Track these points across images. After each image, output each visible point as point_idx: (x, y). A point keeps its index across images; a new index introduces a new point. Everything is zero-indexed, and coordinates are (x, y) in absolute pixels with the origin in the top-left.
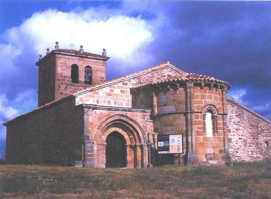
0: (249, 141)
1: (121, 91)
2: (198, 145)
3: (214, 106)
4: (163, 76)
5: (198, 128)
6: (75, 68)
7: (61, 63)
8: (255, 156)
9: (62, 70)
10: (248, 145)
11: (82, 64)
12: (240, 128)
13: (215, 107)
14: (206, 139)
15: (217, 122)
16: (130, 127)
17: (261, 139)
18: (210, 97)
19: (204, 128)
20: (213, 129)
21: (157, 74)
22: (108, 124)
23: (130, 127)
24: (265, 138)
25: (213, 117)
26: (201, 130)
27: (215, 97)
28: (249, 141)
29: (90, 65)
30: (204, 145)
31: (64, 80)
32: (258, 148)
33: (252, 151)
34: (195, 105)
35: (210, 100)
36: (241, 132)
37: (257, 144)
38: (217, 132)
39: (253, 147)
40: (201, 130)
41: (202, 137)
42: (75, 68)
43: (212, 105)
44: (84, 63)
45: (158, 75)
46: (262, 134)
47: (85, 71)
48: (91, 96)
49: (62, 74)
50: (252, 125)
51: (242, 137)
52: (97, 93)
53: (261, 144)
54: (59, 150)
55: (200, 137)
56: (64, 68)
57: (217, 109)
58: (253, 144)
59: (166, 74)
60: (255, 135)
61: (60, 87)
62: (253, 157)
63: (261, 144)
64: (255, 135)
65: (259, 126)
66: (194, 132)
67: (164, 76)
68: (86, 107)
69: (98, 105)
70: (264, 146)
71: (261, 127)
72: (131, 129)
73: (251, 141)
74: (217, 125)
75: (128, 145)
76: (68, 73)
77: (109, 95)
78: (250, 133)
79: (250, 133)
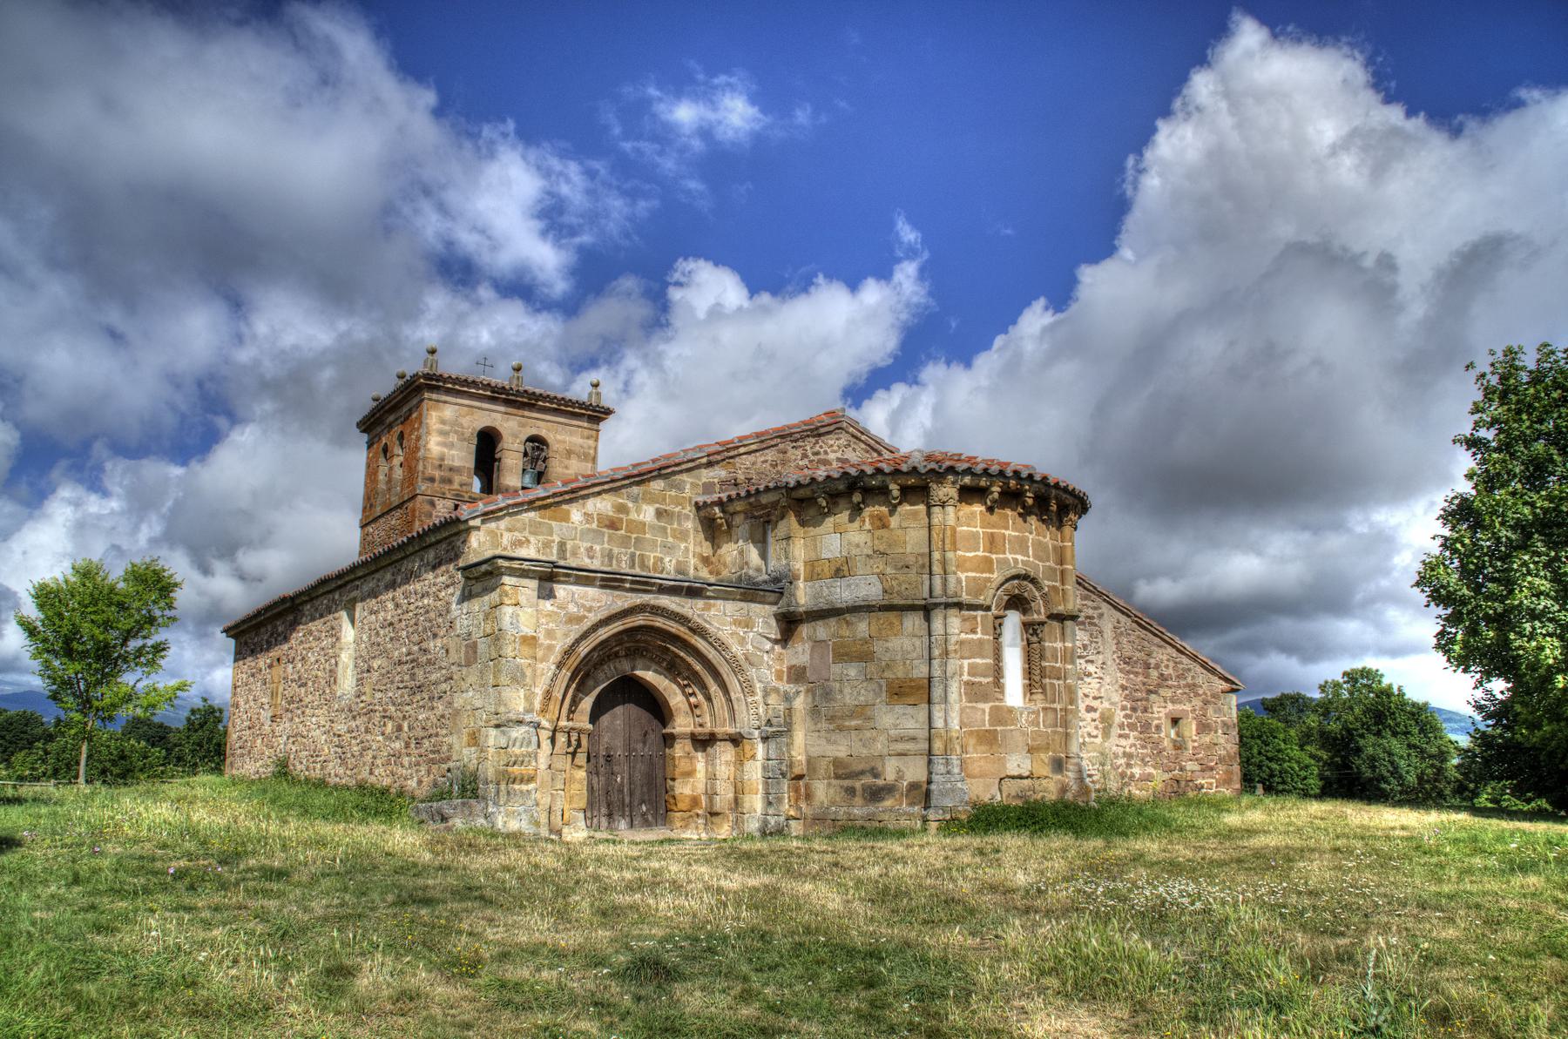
0: (1119, 717)
1: (659, 514)
2: (972, 741)
3: (1033, 581)
4: (819, 461)
5: (973, 670)
6: (487, 443)
7: (443, 422)
8: (1137, 771)
9: (444, 444)
10: (1116, 731)
11: (513, 429)
12: (1091, 668)
13: (1039, 588)
14: (1003, 715)
15: (1043, 649)
16: (690, 660)
17: (1160, 712)
18: (1021, 546)
19: (998, 671)
20: (1028, 673)
21: (799, 453)
22: (595, 627)
23: (690, 660)
24: (1170, 706)
25: (1030, 628)
26: (985, 680)
27: (1039, 546)
28: (1119, 717)
29: (543, 433)
30: (995, 738)
31: (450, 481)
32: (1145, 742)
33: (1128, 756)
34: (963, 576)
35: (1020, 557)
36: (1094, 683)
37: (1146, 727)
38: (1043, 687)
39: (1132, 740)
40: (985, 680)
41: (987, 707)
42: (487, 443)
43: (1026, 577)
44: (523, 425)
45: (805, 456)
46: (1161, 691)
47: (526, 454)
48: (535, 529)
49: (442, 459)
50: (1127, 661)
51: (1095, 704)
52: (566, 518)
53: (1158, 727)
54: (397, 745)
55: (981, 705)
56: (453, 438)
57: (1044, 596)
58: (1132, 727)
59: (832, 456)
60: (1139, 695)
61: (433, 504)
62: (1132, 776)
63: (1158, 727)
64: (1139, 695)
65: (1152, 661)
66: (955, 690)
67: (826, 462)
68: (513, 572)
69: (562, 563)
70: (1168, 736)
71: (1157, 667)
72: (698, 667)
73: (1126, 716)
74: (1042, 657)
75: (683, 736)
76: (463, 456)
77: (613, 525)
78: (1124, 688)
79: (1124, 688)
